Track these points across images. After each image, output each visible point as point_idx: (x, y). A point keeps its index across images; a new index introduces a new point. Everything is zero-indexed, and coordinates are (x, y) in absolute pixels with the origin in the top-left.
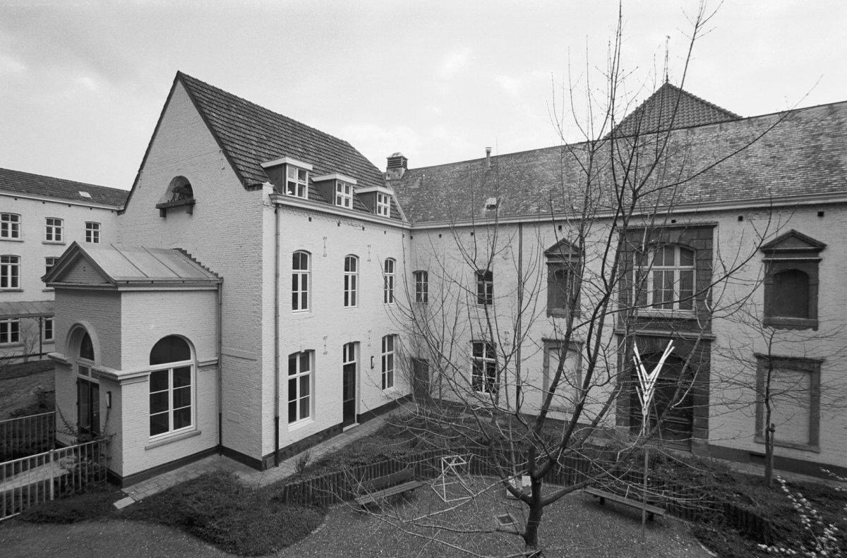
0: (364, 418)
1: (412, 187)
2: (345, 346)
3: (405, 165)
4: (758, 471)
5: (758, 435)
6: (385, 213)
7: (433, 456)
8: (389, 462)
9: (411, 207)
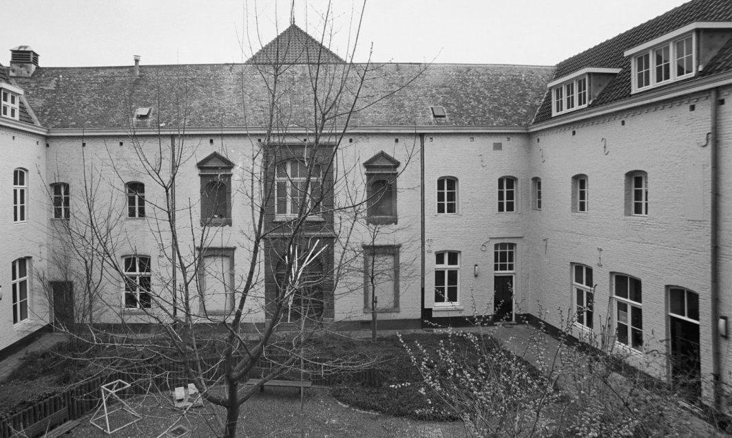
1: (45, 88)
3: (35, 61)
4: (367, 334)
5: (366, 307)
6: (13, 115)
7: (92, 389)
8: (34, 408)
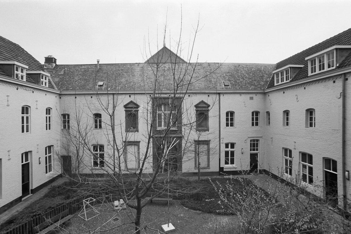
0: (34, 191)
1: (59, 73)
2: (22, 154)
3: (55, 62)
5: (196, 166)
6: (46, 85)
7: (79, 201)
9: (59, 83)
